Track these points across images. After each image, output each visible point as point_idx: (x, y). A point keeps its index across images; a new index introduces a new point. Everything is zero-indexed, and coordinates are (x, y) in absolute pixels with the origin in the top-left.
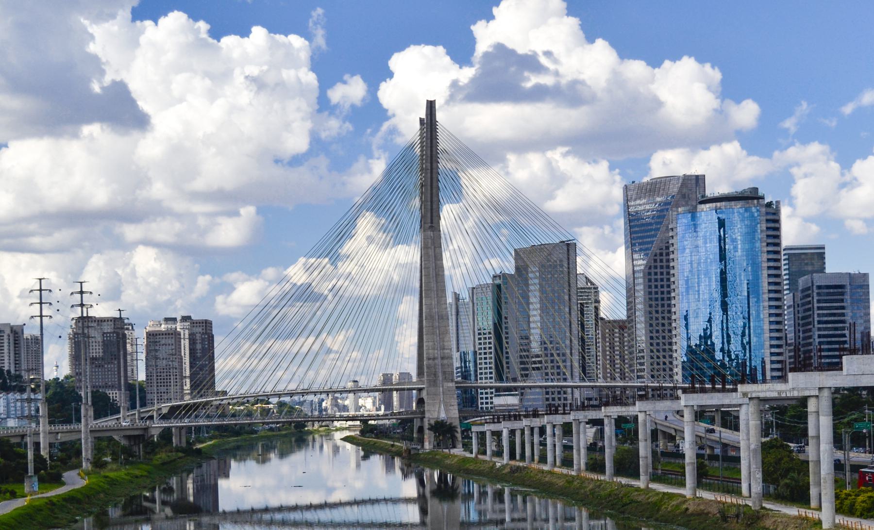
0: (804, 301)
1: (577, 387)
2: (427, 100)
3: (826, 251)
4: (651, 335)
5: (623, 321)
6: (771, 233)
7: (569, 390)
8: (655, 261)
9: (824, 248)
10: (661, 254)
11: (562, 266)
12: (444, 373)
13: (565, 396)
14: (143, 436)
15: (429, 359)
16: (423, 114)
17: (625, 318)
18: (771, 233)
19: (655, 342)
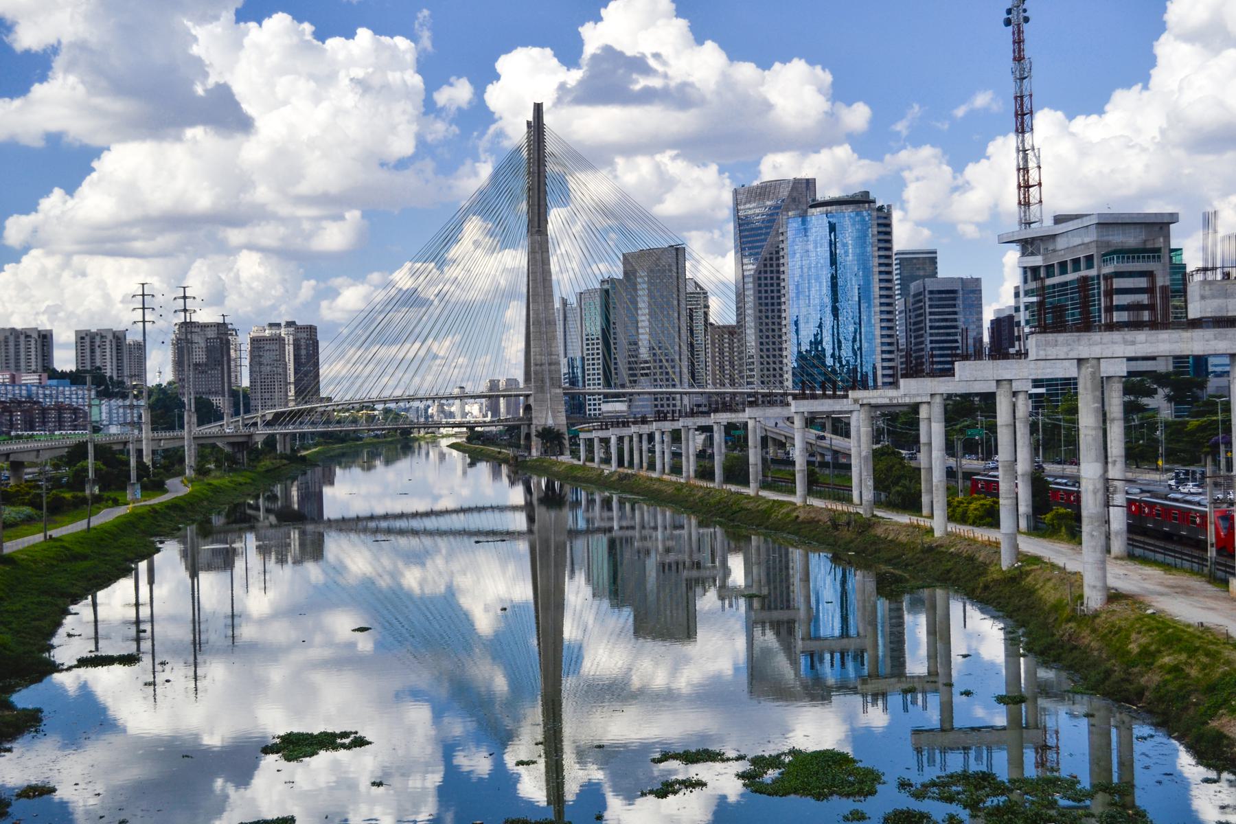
1: (686, 393)
3: (938, 255)
7: (678, 396)
8: (765, 265)
9: (936, 253)
10: (771, 259)
11: (670, 271)
12: (552, 379)
14: (247, 443)
17: (734, 323)
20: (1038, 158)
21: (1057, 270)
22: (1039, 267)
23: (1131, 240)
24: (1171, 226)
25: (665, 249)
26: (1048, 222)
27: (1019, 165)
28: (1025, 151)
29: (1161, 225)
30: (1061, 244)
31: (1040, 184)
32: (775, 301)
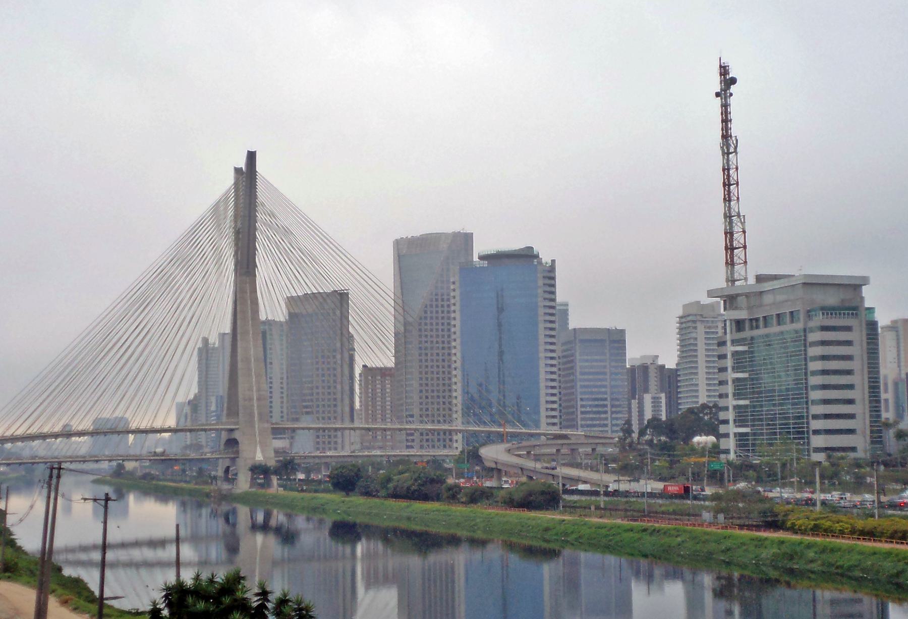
0: (565, 353)
2: (248, 151)
4: (421, 382)
5: (390, 369)
6: (548, 289)
7: (339, 434)
8: (426, 312)
10: (431, 306)
13: (335, 440)
15: (245, 400)
16: (242, 164)
18: (548, 289)
19: (424, 388)
20: (743, 223)
21: (761, 323)
22: (746, 319)
23: (832, 299)
24: (863, 287)
25: (328, 294)
26: (752, 281)
27: (725, 229)
28: (731, 217)
29: (855, 287)
30: (768, 299)
31: (745, 247)
32: (446, 345)
